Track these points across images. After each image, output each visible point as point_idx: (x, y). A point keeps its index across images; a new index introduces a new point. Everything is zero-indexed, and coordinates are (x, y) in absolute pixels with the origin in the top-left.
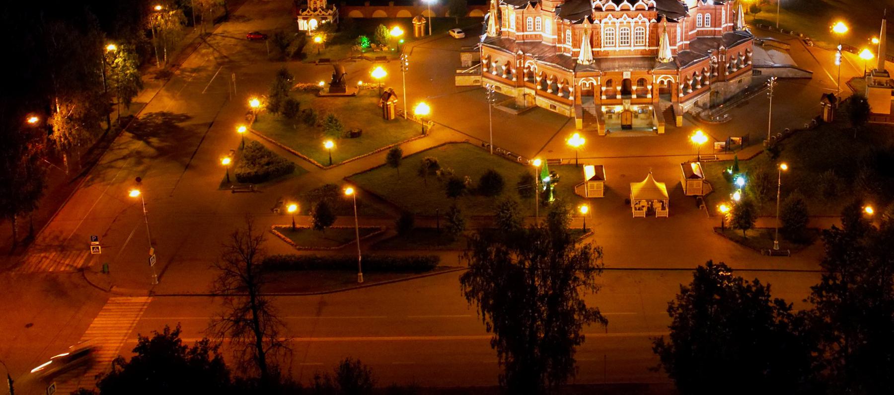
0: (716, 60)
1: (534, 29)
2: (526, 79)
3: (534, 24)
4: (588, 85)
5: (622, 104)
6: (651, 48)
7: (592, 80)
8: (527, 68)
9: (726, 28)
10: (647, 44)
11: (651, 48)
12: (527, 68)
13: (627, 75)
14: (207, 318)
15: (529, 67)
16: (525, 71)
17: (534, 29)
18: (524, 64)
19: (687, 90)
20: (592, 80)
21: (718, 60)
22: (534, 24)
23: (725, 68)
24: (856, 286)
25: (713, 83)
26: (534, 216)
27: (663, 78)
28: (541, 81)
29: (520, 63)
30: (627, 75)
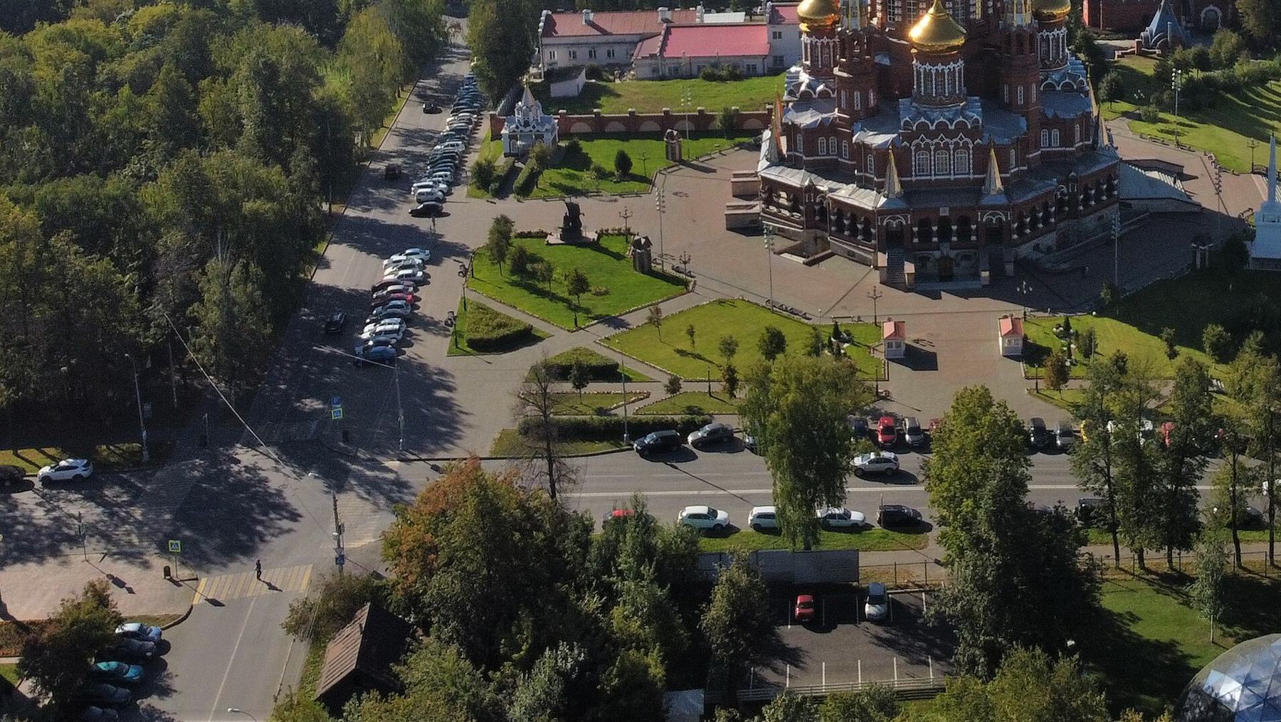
0: (1065, 190)
1: (828, 150)
2: (817, 218)
3: (828, 146)
4: (994, 221)
5: (939, 249)
6: (976, 176)
7: (998, 214)
8: (818, 204)
9: (1080, 148)
10: (971, 171)
11: (976, 176)
12: (818, 204)
13: (944, 212)
14: (850, 489)
15: (821, 203)
16: (817, 208)
17: (828, 150)
18: (815, 198)
19: (315, 244)
20: (998, 214)
21: (1068, 190)
22: (828, 146)
23: (1078, 200)
24: (254, 505)
25: (1060, 221)
26: (709, 392)
27: (990, 214)
28: (836, 220)
29: (810, 199)
30: (944, 211)
